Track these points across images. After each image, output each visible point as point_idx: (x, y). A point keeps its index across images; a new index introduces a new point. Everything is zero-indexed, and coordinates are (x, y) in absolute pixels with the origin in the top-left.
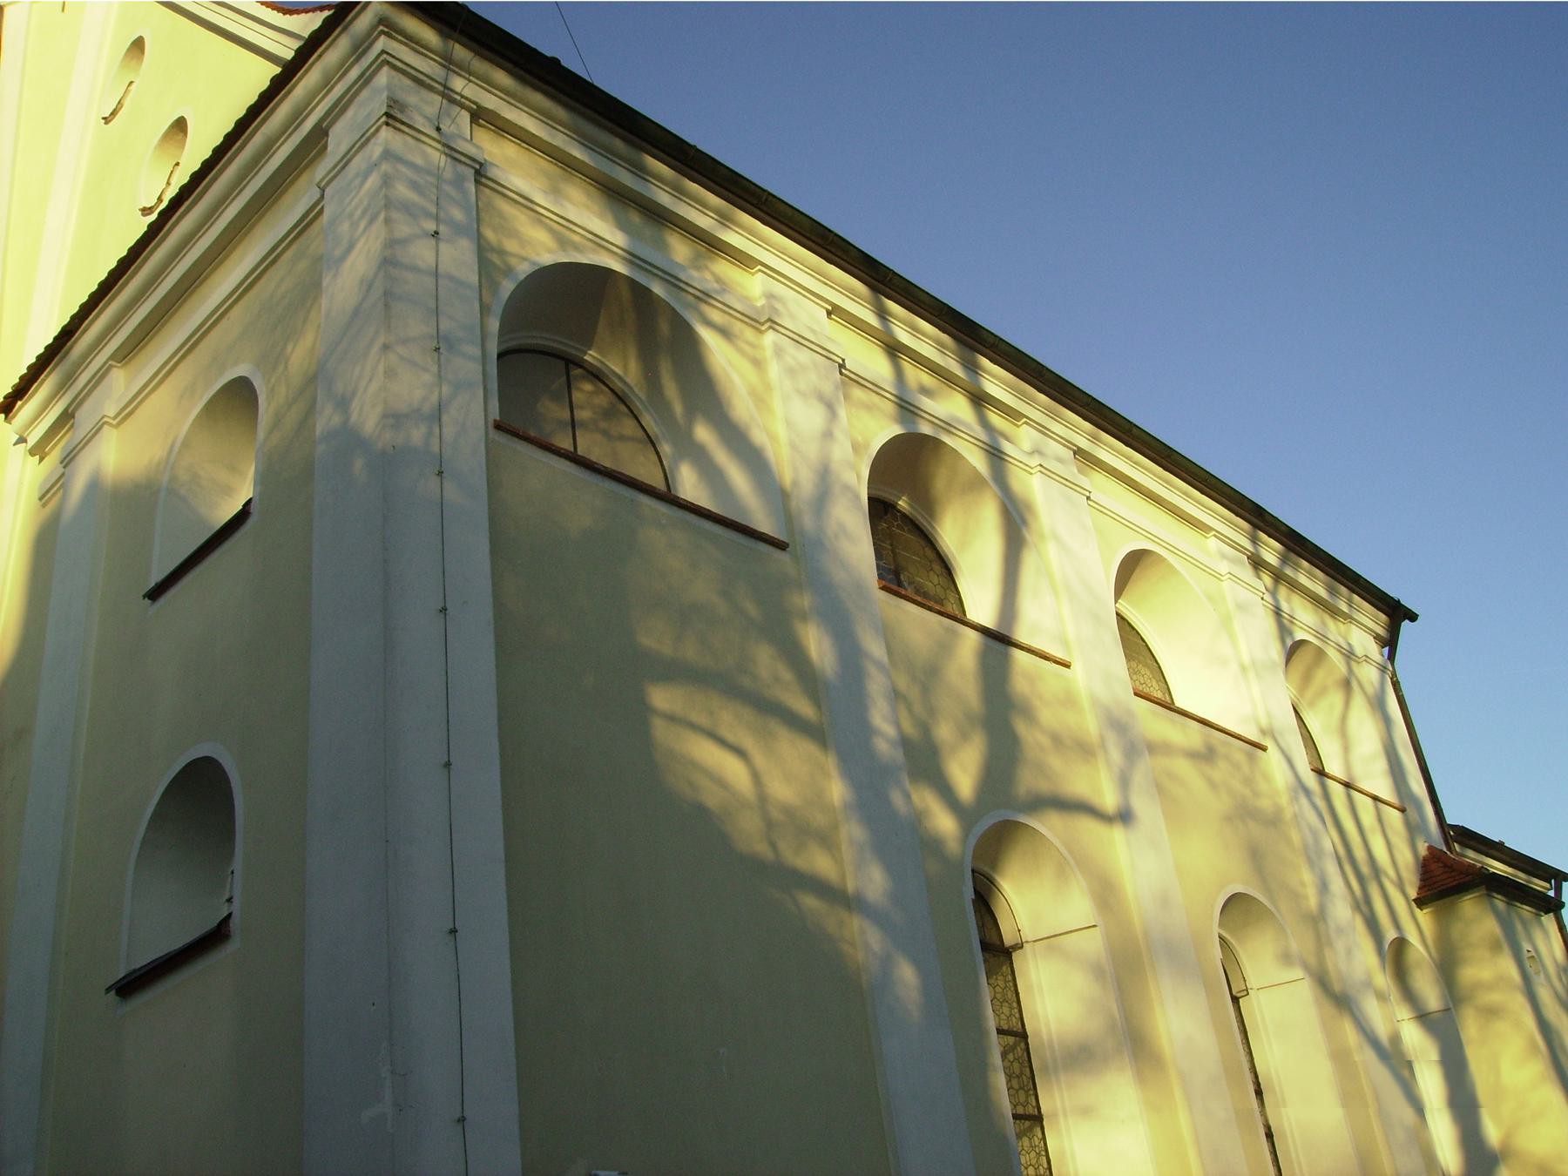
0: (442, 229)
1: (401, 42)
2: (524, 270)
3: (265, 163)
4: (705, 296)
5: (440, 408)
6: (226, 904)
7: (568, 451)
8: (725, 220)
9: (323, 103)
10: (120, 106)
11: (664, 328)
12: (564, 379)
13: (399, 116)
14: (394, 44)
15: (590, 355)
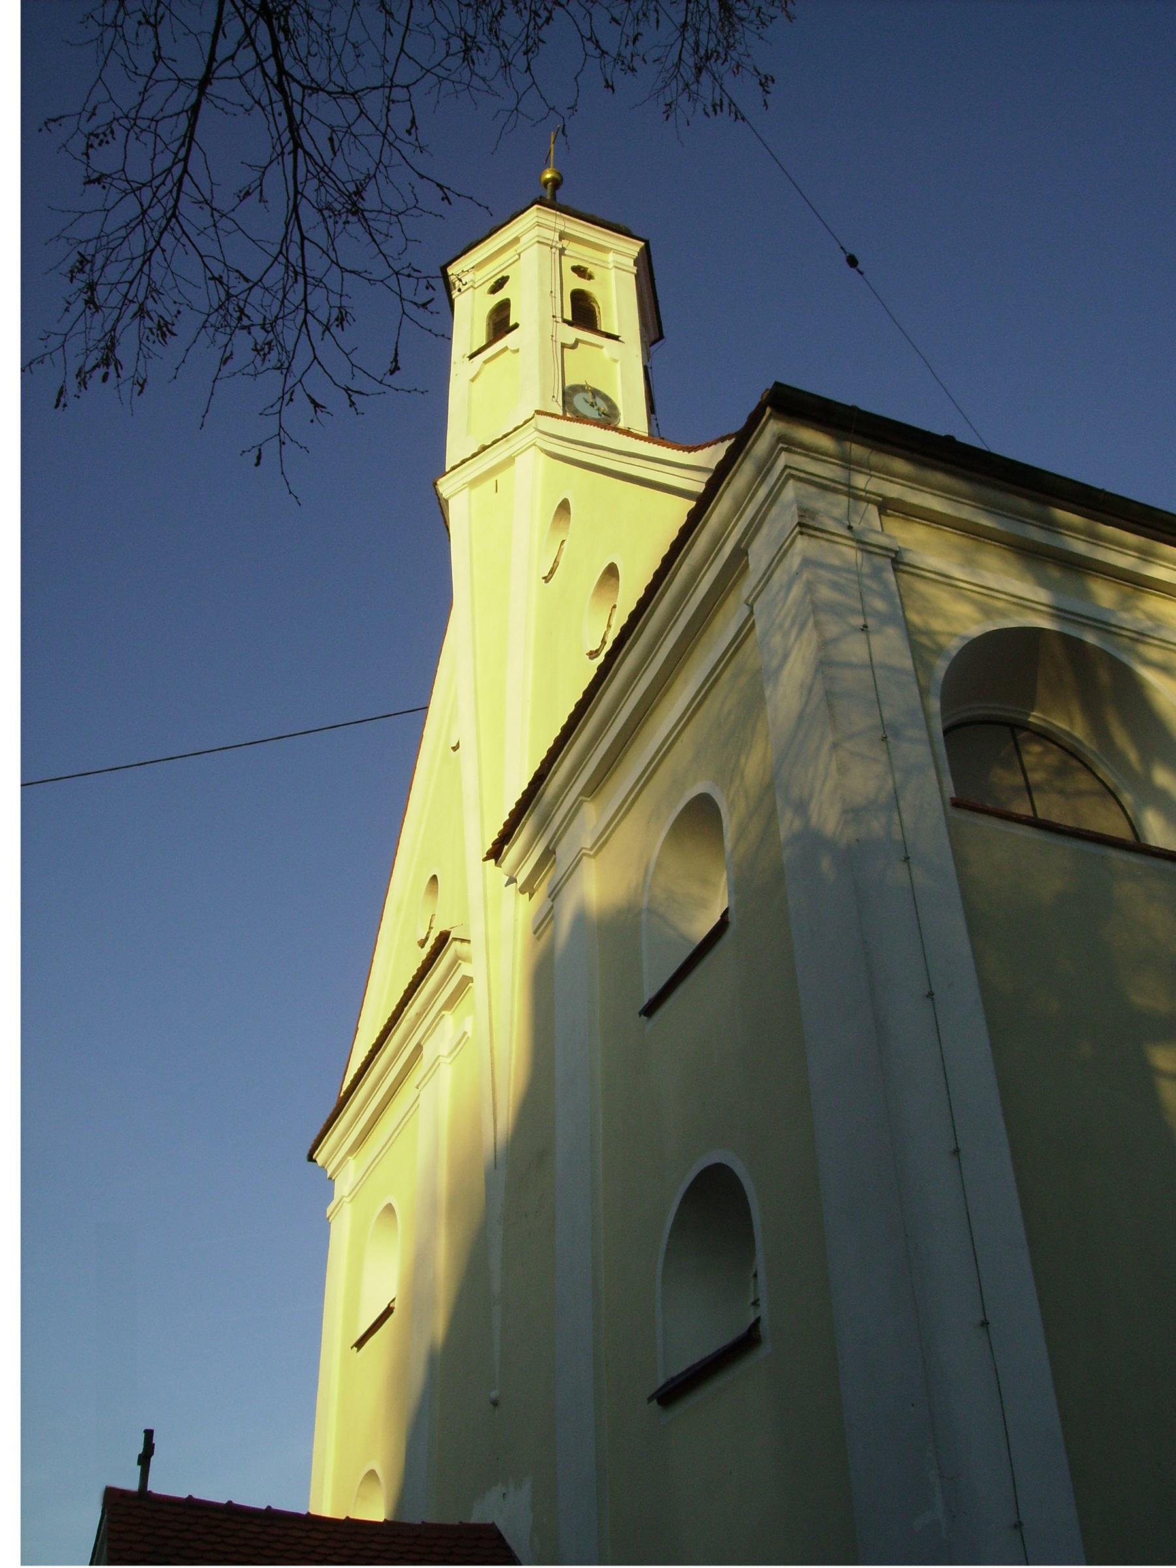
0: (871, 622)
1: (800, 454)
2: (954, 646)
3: (694, 592)
4: (1141, 637)
5: (896, 796)
6: (753, 1307)
7: (1028, 817)
8: (1147, 556)
9: (740, 523)
10: (556, 564)
11: (1104, 676)
12: (1012, 743)
13: (811, 523)
14: (797, 458)
15: (1034, 716)
